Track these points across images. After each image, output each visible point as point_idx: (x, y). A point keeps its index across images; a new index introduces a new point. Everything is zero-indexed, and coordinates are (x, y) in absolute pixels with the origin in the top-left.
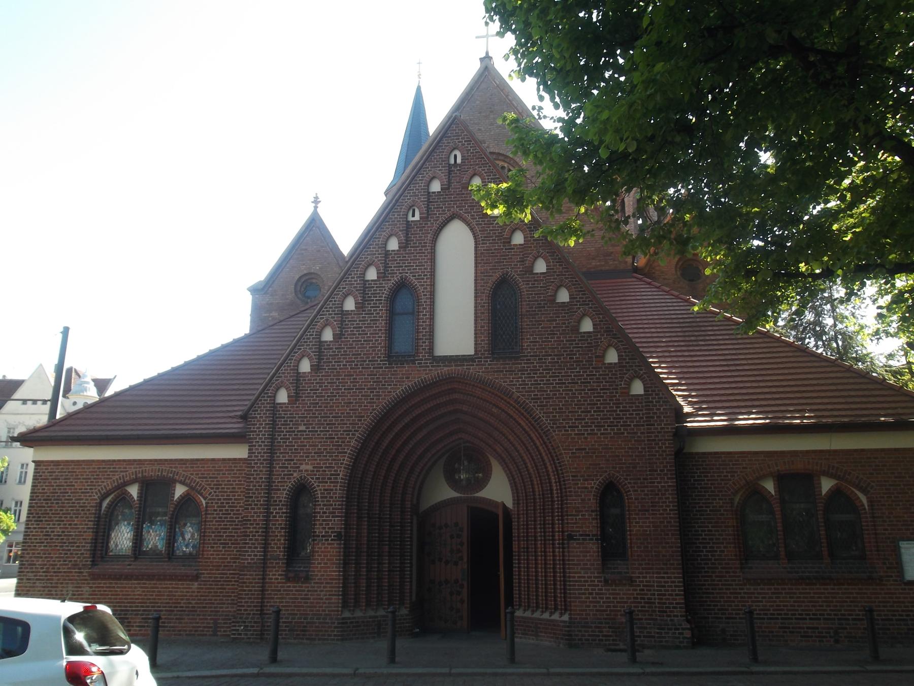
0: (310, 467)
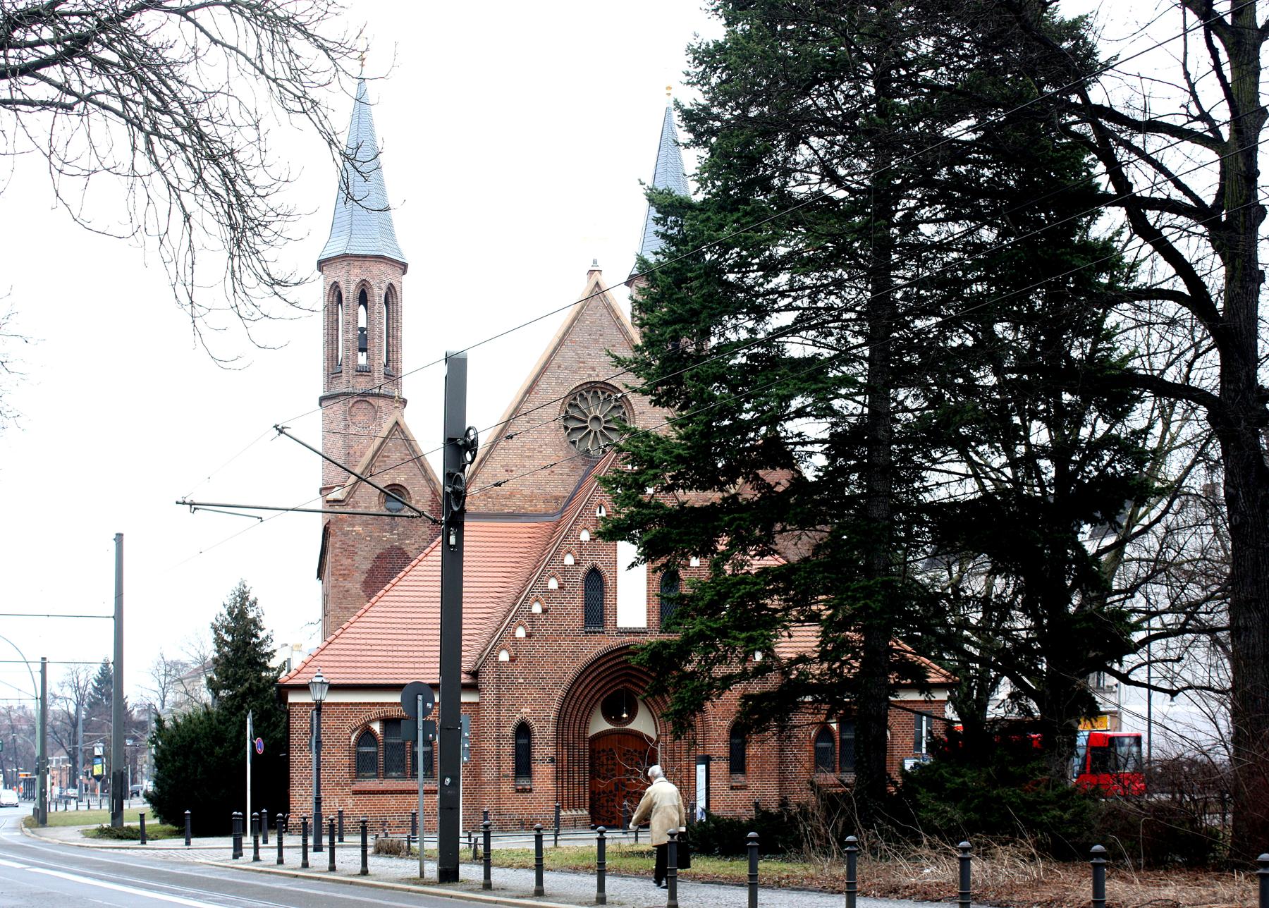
0: (528, 710)
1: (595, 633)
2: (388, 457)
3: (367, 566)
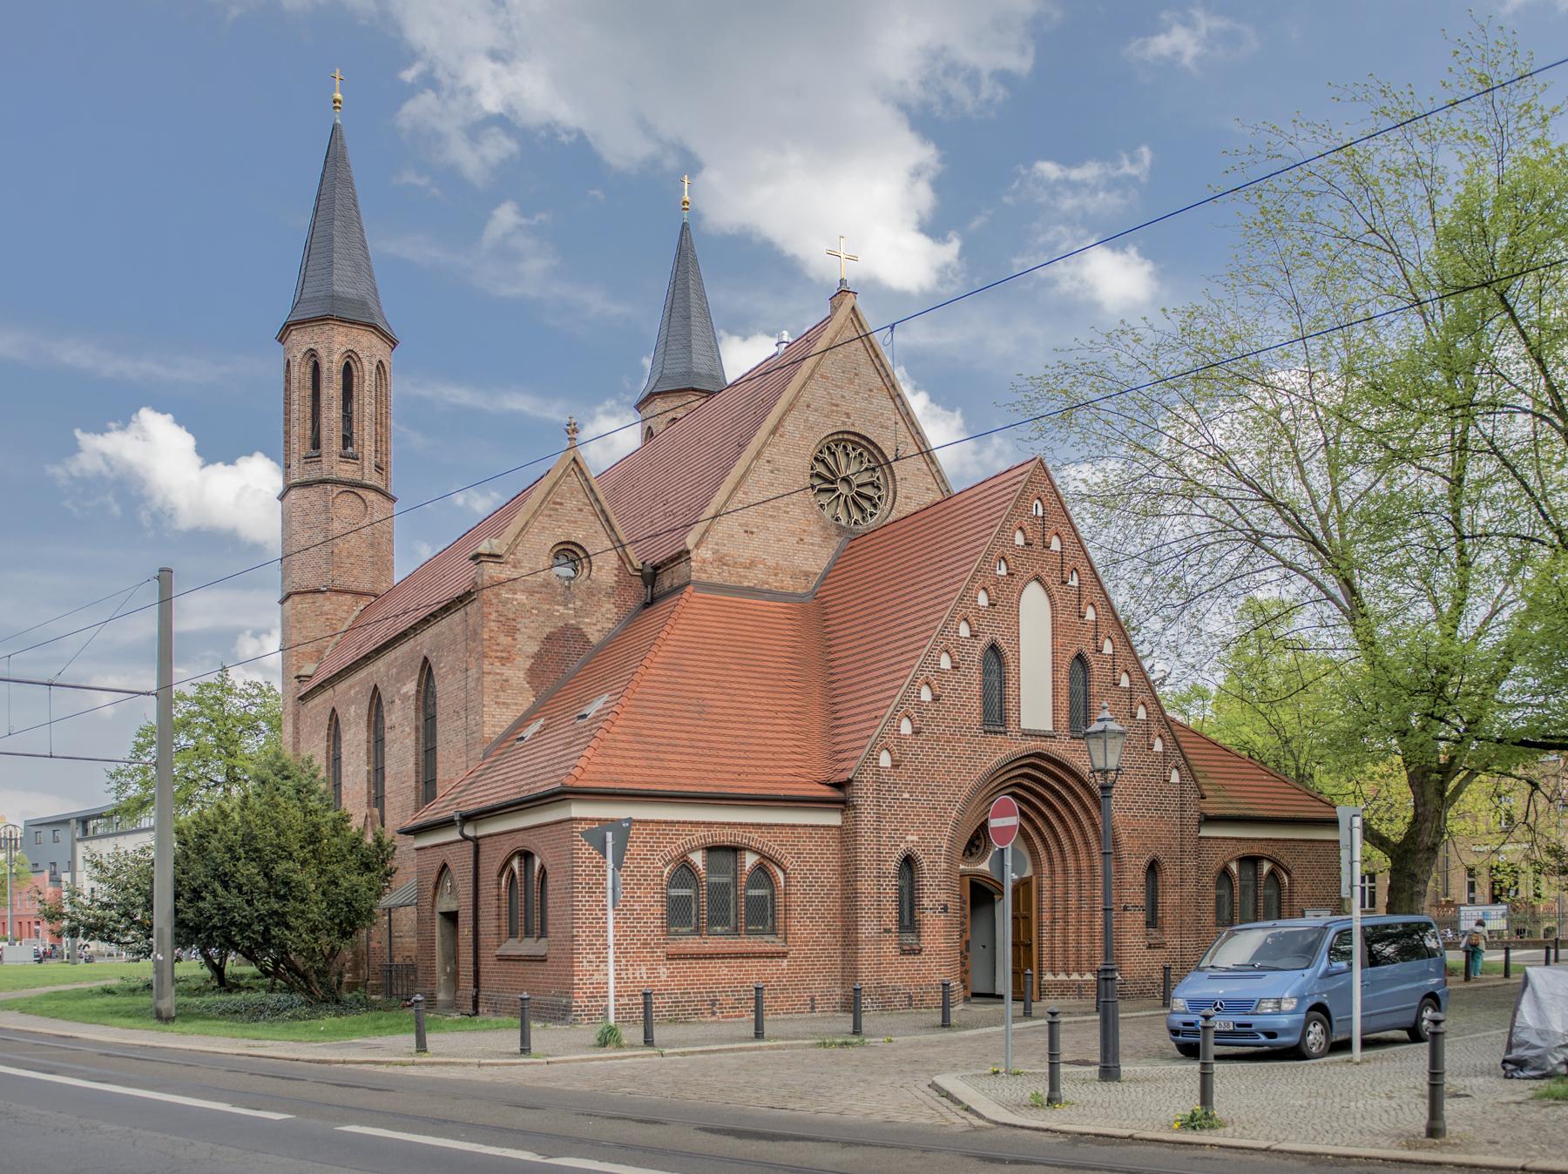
0: (915, 838)
1: (996, 733)
2: (561, 504)
3: (533, 648)
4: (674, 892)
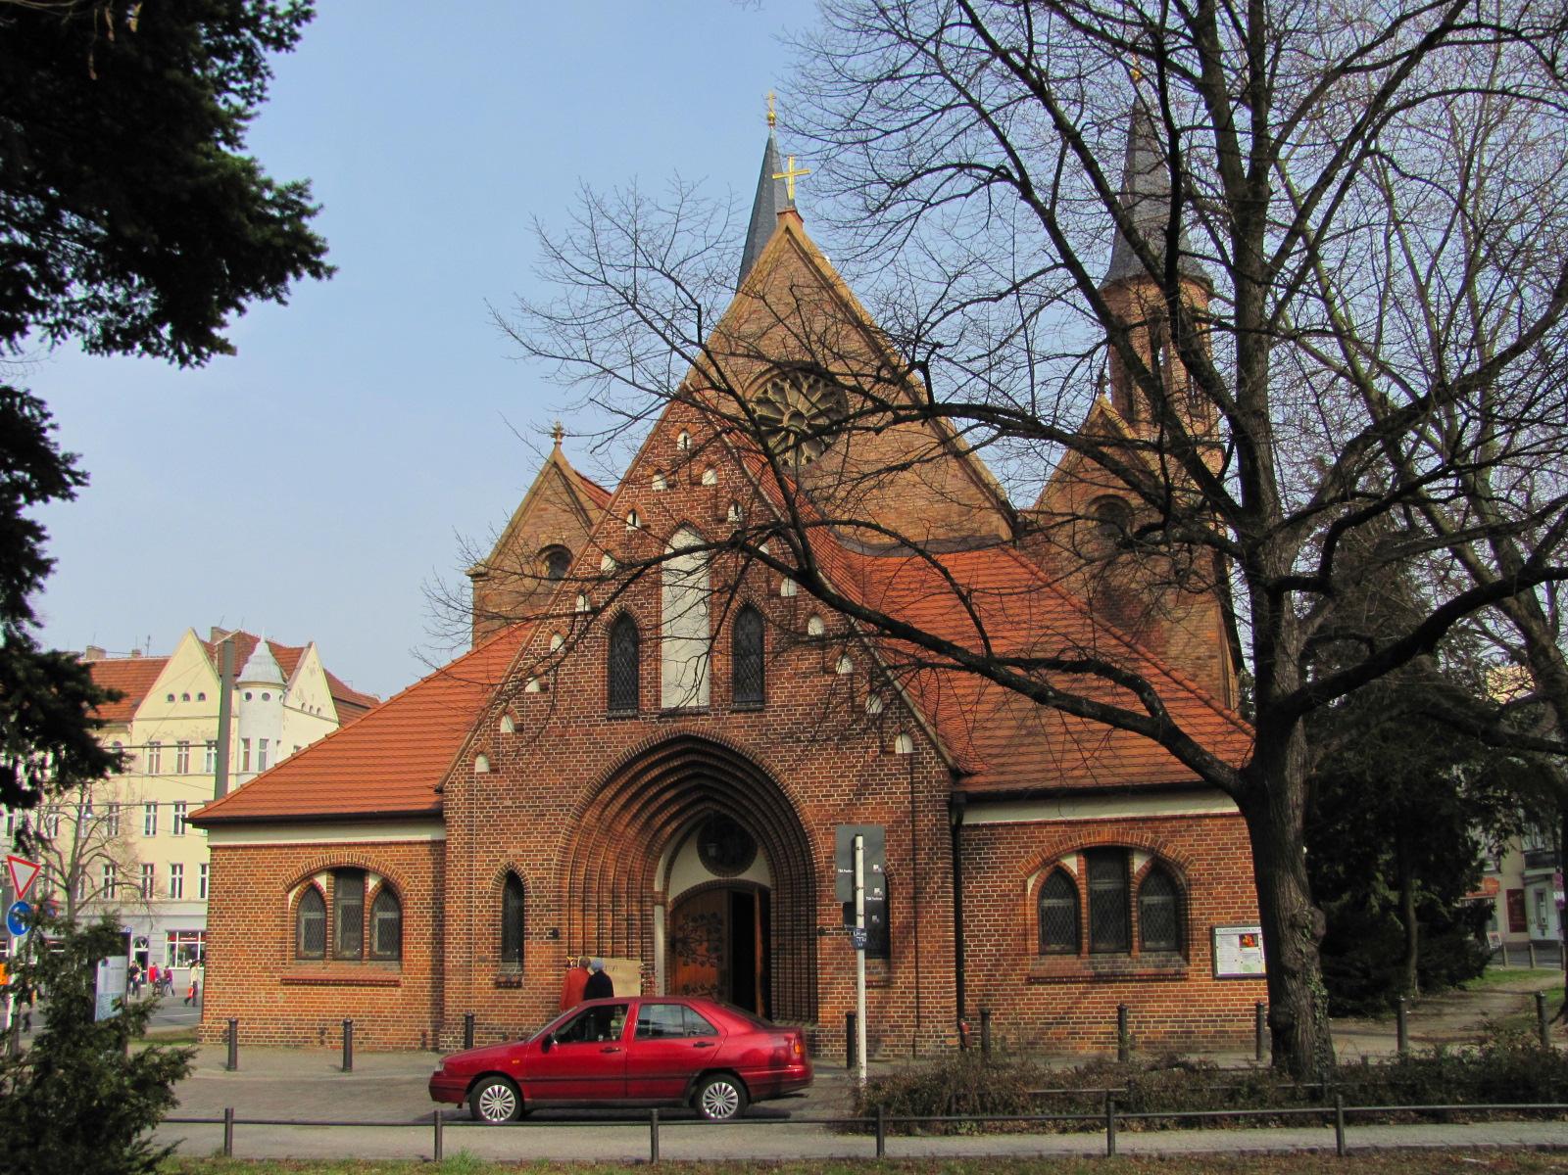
1: (623, 718)
4: (1048, 903)
